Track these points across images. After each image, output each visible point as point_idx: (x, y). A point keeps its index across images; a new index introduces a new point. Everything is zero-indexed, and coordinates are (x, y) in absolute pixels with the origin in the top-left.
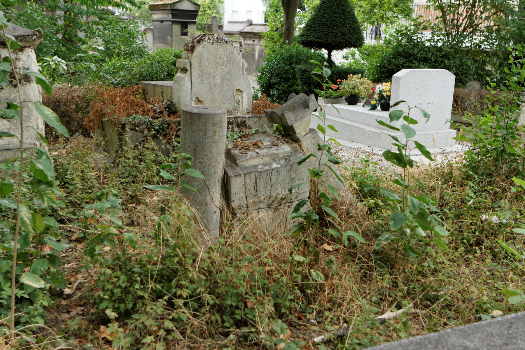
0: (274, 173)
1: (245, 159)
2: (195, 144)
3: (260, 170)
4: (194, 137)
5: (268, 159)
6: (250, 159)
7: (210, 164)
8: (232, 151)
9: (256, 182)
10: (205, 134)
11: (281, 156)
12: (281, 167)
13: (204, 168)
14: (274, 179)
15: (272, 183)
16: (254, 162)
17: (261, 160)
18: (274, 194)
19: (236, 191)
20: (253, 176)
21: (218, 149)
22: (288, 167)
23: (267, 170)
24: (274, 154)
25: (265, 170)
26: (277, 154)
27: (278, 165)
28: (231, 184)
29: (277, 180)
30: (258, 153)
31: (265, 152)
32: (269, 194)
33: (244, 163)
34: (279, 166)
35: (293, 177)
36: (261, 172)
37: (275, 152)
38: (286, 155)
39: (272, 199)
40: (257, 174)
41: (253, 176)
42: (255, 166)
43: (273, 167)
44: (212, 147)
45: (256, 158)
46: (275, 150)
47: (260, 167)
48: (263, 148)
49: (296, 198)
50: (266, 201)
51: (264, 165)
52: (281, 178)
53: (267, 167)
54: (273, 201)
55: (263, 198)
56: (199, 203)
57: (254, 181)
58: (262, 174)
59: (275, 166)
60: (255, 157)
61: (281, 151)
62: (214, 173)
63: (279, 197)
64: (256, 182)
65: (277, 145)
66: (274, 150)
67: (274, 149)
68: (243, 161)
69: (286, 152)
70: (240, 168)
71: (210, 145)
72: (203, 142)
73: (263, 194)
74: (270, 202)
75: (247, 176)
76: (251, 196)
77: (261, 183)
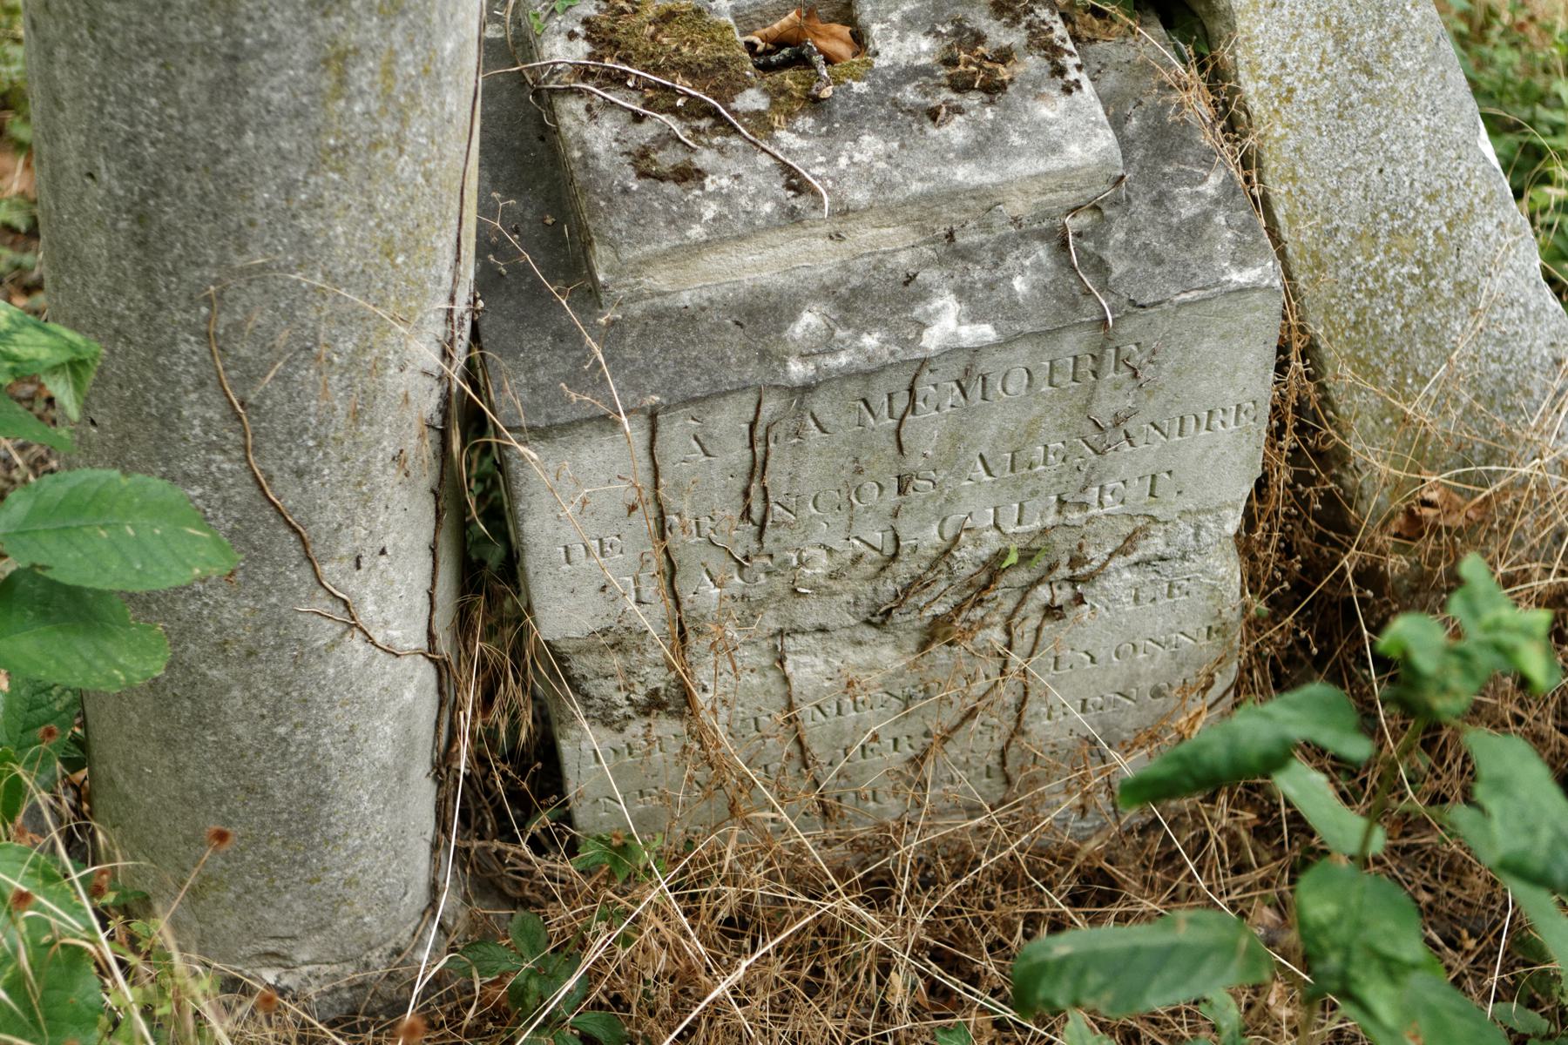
0: (938, 391)
1: (668, 241)
2: (137, 164)
3: (797, 370)
4: (127, 101)
5: (897, 244)
6: (720, 236)
7: (307, 349)
8: (570, 113)
9: (758, 468)
10: (228, 87)
11: (1018, 205)
12: (1006, 343)
13: (250, 378)
14: (928, 431)
15: (914, 462)
16: (757, 266)
17: (784, 539)
18: (931, 538)
19: (569, 534)
20: (730, 419)
21: (384, 204)
22: (1073, 343)
23: (866, 375)
24: (953, 195)
25: (847, 375)
26: (978, 193)
27: (975, 317)
28: (522, 490)
29: (957, 438)
30: (796, 183)
31: (865, 174)
32: (876, 538)
33: (659, 279)
34: (986, 332)
35: (1103, 410)
36: (807, 389)
37: (965, 174)
38: (1070, 197)
39: (904, 570)
40: (771, 406)
41: (730, 419)
42: (762, 314)
43: (932, 340)
44: (315, 204)
45: (776, 237)
46: (966, 154)
47: (809, 320)
48: (855, 121)
49: (1122, 551)
50: (857, 585)
51: (851, 301)
52: (993, 426)
53: (870, 341)
54: (917, 584)
55: (821, 565)
56: (222, 647)
57: (739, 454)
58: (820, 404)
59: (947, 324)
60: (771, 225)
61: (1022, 167)
62: (356, 415)
63: (968, 558)
64: (758, 468)
65: (993, 89)
66: (950, 157)
67: (956, 132)
68: (647, 262)
69: (1066, 178)
70: (613, 335)
71: (289, 187)
72: (217, 155)
73: (821, 542)
74: (889, 587)
75: (677, 431)
76: (717, 562)
77: (804, 469)
